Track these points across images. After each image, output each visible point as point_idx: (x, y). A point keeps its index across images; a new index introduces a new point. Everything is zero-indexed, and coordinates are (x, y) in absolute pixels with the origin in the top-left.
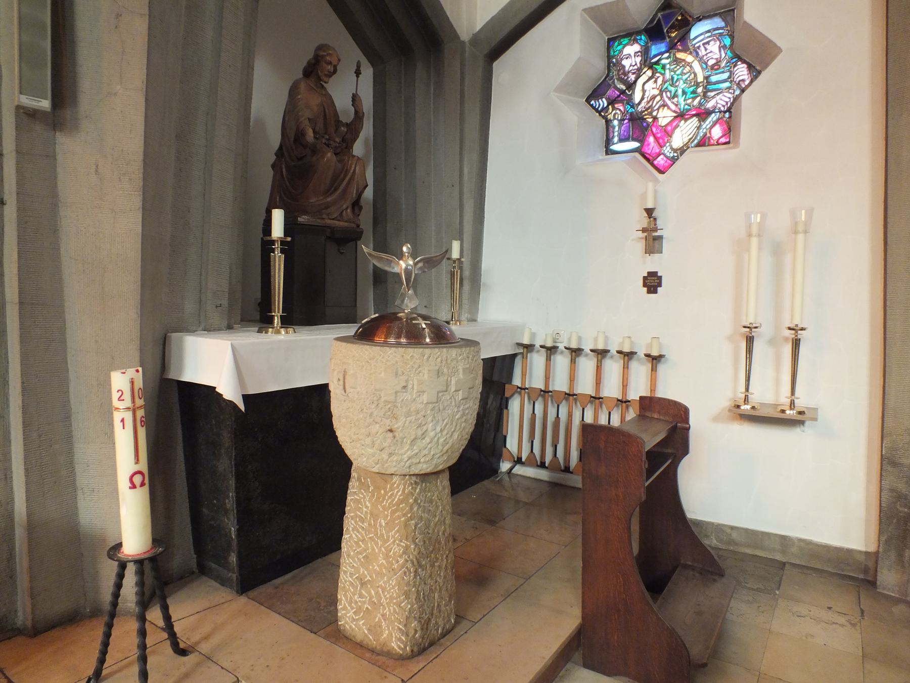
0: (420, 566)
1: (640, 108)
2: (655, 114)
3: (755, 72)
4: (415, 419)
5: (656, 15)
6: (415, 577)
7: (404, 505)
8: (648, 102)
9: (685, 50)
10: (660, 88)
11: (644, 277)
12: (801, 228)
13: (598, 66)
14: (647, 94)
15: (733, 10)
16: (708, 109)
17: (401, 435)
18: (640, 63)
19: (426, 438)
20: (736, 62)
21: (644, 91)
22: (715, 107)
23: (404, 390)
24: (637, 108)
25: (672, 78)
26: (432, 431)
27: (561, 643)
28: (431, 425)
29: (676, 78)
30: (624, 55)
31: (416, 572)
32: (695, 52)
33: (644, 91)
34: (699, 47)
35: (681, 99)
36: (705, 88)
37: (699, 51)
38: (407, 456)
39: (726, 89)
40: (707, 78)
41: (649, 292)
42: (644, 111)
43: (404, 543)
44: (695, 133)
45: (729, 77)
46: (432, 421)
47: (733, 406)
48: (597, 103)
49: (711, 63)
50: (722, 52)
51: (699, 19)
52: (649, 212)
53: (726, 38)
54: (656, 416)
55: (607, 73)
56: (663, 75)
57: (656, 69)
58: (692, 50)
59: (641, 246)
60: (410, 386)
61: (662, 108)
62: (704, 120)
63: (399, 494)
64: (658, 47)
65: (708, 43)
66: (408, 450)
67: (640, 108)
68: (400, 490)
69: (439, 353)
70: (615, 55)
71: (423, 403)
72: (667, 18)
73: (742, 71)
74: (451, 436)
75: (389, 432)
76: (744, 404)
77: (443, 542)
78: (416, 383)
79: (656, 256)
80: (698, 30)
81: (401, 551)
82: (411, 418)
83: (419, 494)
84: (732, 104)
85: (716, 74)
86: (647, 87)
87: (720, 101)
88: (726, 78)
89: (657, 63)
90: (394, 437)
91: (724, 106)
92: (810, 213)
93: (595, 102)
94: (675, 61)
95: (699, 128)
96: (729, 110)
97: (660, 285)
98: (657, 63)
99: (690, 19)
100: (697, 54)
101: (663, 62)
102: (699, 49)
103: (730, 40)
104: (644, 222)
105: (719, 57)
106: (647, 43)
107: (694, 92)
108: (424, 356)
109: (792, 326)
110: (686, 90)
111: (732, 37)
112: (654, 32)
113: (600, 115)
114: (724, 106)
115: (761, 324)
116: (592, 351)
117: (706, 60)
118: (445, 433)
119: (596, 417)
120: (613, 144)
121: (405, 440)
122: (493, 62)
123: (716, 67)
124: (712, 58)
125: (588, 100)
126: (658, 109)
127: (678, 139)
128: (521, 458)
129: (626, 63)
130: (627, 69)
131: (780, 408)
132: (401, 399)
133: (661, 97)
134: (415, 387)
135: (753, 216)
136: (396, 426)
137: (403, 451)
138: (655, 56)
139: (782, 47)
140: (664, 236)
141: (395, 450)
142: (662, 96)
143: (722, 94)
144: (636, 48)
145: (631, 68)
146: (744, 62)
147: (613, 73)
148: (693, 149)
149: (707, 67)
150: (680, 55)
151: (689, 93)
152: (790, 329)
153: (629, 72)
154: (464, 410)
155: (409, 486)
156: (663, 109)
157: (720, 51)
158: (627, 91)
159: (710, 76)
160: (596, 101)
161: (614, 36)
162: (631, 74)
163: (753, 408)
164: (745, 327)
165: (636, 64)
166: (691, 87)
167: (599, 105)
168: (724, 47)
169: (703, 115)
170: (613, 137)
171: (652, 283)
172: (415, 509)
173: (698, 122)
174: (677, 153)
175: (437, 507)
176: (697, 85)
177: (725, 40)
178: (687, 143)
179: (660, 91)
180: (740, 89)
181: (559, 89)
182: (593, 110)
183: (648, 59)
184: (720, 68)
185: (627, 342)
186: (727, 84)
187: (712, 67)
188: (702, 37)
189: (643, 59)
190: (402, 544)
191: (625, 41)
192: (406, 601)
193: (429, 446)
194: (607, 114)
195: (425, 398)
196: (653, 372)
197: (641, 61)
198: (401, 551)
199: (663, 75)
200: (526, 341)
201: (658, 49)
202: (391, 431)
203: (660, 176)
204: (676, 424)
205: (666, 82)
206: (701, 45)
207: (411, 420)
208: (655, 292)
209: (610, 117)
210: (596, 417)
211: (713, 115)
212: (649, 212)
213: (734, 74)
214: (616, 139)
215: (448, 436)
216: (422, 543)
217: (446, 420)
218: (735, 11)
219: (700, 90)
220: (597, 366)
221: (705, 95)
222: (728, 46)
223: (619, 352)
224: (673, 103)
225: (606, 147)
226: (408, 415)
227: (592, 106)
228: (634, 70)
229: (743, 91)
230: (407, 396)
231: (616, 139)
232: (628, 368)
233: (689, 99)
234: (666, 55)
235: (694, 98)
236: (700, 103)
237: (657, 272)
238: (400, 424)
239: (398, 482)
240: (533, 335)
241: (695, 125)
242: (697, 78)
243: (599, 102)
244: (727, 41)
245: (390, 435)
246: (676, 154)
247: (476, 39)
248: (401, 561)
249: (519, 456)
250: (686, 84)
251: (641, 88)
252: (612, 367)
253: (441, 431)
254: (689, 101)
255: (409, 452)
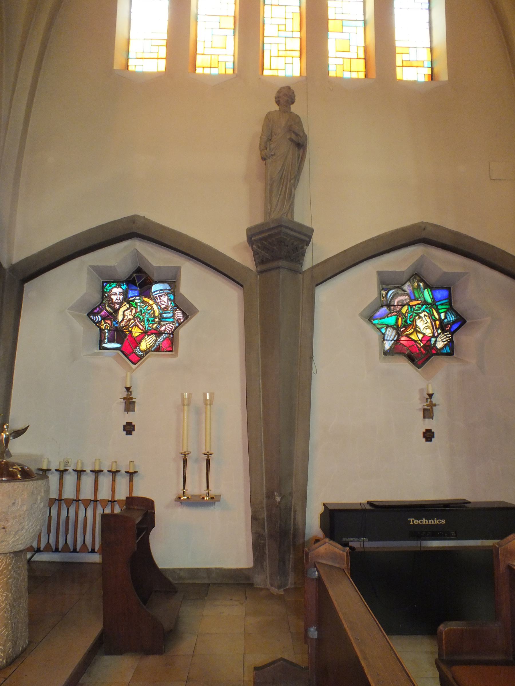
0: (14, 607)
1: (121, 325)
2: (130, 329)
3: (186, 317)
4: (19, 520)
5: (132, 275)
6: (11, 613)
7: (6, 571)
8: (126, 322)
9: (149, 297)
10: (134, 316)
11: (124, 425)
12: (208, 403)
13: (96, 297)
14: (126, 317)
15: (175, 282)
16: (161, 331)
17: (10, 530)
18: (122, 299)
19: (24, 530)
20: (176, 309)
21: (124, 315)
22: (164, 331)
23: (13, 505)
24: (120, 324)
25: (141, 311)
26: (27, 525)
27: (395, 270)
28: (27, 522)
29: (143, 311)
30: (113, 293)
31: (11, 611)
32: (154, 299)
33: (124, 315)
34: (156, 297)
35: (146, 324)
36: (160, 319)
37: (156, 299)
38: (12, 541)
39: (170, 322)
40: (161, 314)
41: (127, 434)
42: (124, 327)
43: (5, 593)
44: (154, 343)
45: (173, 316)
46: (28, 520)
47: (177, 497)
48: (95, 318)
49: (163, 306)
50: (169, 302)
51: (156, 282)
52: (128, 389)
53: (171, 295)
54: (136, 507)
55: (101, 301)
56: (136, 308)
57: (132, 304)
58: (152, 298)
59: (122, 406)
60: (17, 502)
61: (135, 327)
62: (159, 337)
63: (3, 565)
64: (133, 293)
65: (161, 296)
66: (12, 538)
67: (121, 325)
68: (4, 562)
69: (32, 484)
70: (107, 292)
71: (23, 511)
72: (139, 278)
73: (179, 314)
74: (36, 528)
75: (3, 529)
76: (183, 496)
77: (24, 592)
78: (20, 500)
79: (131, 413)
80: (156, 287)
81: (3, 599)
82: (16, 520)
83: (14, 564)
84: (174, 330)
85: (166, 313)
86: (126, 313)
87: (167, 327)
88: (171, 316)
89: (133, 301)
90: (6, 531)
91: (169, 331)
92: (212, 395)
93: (93, 317)
94: (142, 302)
95: (156, 341)
96: (172, 333)
97: (134, 430)
98: (133, 301)
99: (152, 281)
100: (156, 301)
101: (136, 301)
102: (156, 298)
103: (173, 296)
104: (125, 394)
105: (167, 304)
106: (127, 289)
107: (153, 321)
108: (24, 486)
109: (206, 452)
110: (149, 319)
111: (174, 295)
112: (130, 282)
113: (96, 325)
114: (169, 331)
115: (190, 452)
116: (74, 470)
117: (160, 305)
118: (34, 525)
119: (112, 510)
120: (105, 343)
121: (11, 533)
122: (25, 283)
123: (166, 309)
124: (164, 304)
125: (89, 315)
126: (132, 327)
127: (144, 346)
128: (40, 548)
129: (114, 298)
130: (114, 301)
131: (202, 497)
132: (11, 510)
133: (134, 321)
134: (20, 503)
135: (185, 394)
136: (7, 525)
137: (9, 539)
138: (132, 297)
139: (199, 310)
140: (136, 402)
141: (5, 539)
142: (135, 321)
143: (169, 324)
144: (119, 290)
145: (117, 301)
146: (180, 309)
147: (105, 302)
148: (153, 353)
149: (161, 308)
150: (146, 299)
151: (151, 321)
152: (204, 454)
153: (115, 303)
154: (43, 513)
155: (9, 559)
156: (135, 327)
157: (168, 302)
158: (113, 314)
159: (162, 313)
160: (94, 316)
161: (107, 281)
162: (116, 304)
163: (188, 498)
164: (182, 454)
165: (120, 299)
166: (152, 317)
167: (96, 319)
168: (170, 300)
169: (158, 334)
170: (105, 339)
171: (129, 428)
172: (12, 572)
173: (155, 337)
174: (143, 353)
175: (22, 571)
176: (155, 317)
177: (171, 296)
178: (149, 348)
179: (134, 317)
180: (178, 323)
181: (72, 308)
182: (92, 322)
183: (127, 298)
184: (167, 310)
185: (114, 464)
186: (172, 320)
187: (163, 309)
188: (158, 292)
189: (124, 298)
190: (4, 594)
191: (114, 285)
192: (5, 630)
193: (25, 534)
194: (100, 325)
195: (25, 508)
196: (131, 482)
197: (122, 298)
198: (3, 599)
199: (136, 308)
200: (45, 467)
201: (133, 293)
202: (4, 528)
203: (134, 366)
204: (148, 511)
205: (137, 312)
206: (158, 296)
207: (17, 520)
208: (131, 434)
209: (103, 327)
210: (112, 510)
211: (164, 335)
212: (128, 389)
213: (175, 315)
214: (106, 341)
215: (35, 528)
216: (15, 593)
217: (35, 519)
218: (176, 282)
219: (157, 320)
220: (95, 481)
221: (159, 323)
222: (172, 300)
223: (109, 471)
224: (141, 325)
225: (99, 345)
226: (15, 518)
227: (91, 319)
228: (118, 302)
229: (180, 324)
230: (14, 508)
231: (106, 341)
232: (115, 480)
233: (150, 324)
234: (138, 298)
235: (153, 324)
236: (156, 327)
237: (132, 423)
238: (10, 524)
239: (2, 558)
240: (49, 463)
241: (154, 339)
242: (155, 313)
243: (95, 317)
244: (172, 297)
245: (3, 530)
246: (142, 354)
247: (13, 268)
248: (3, 605)
249: (39, 547)
250: (149, 316)
251: (122, 314)
252: (105, 481)
253: (32, 525)
254: (151, 325)
255: (13, 539)
